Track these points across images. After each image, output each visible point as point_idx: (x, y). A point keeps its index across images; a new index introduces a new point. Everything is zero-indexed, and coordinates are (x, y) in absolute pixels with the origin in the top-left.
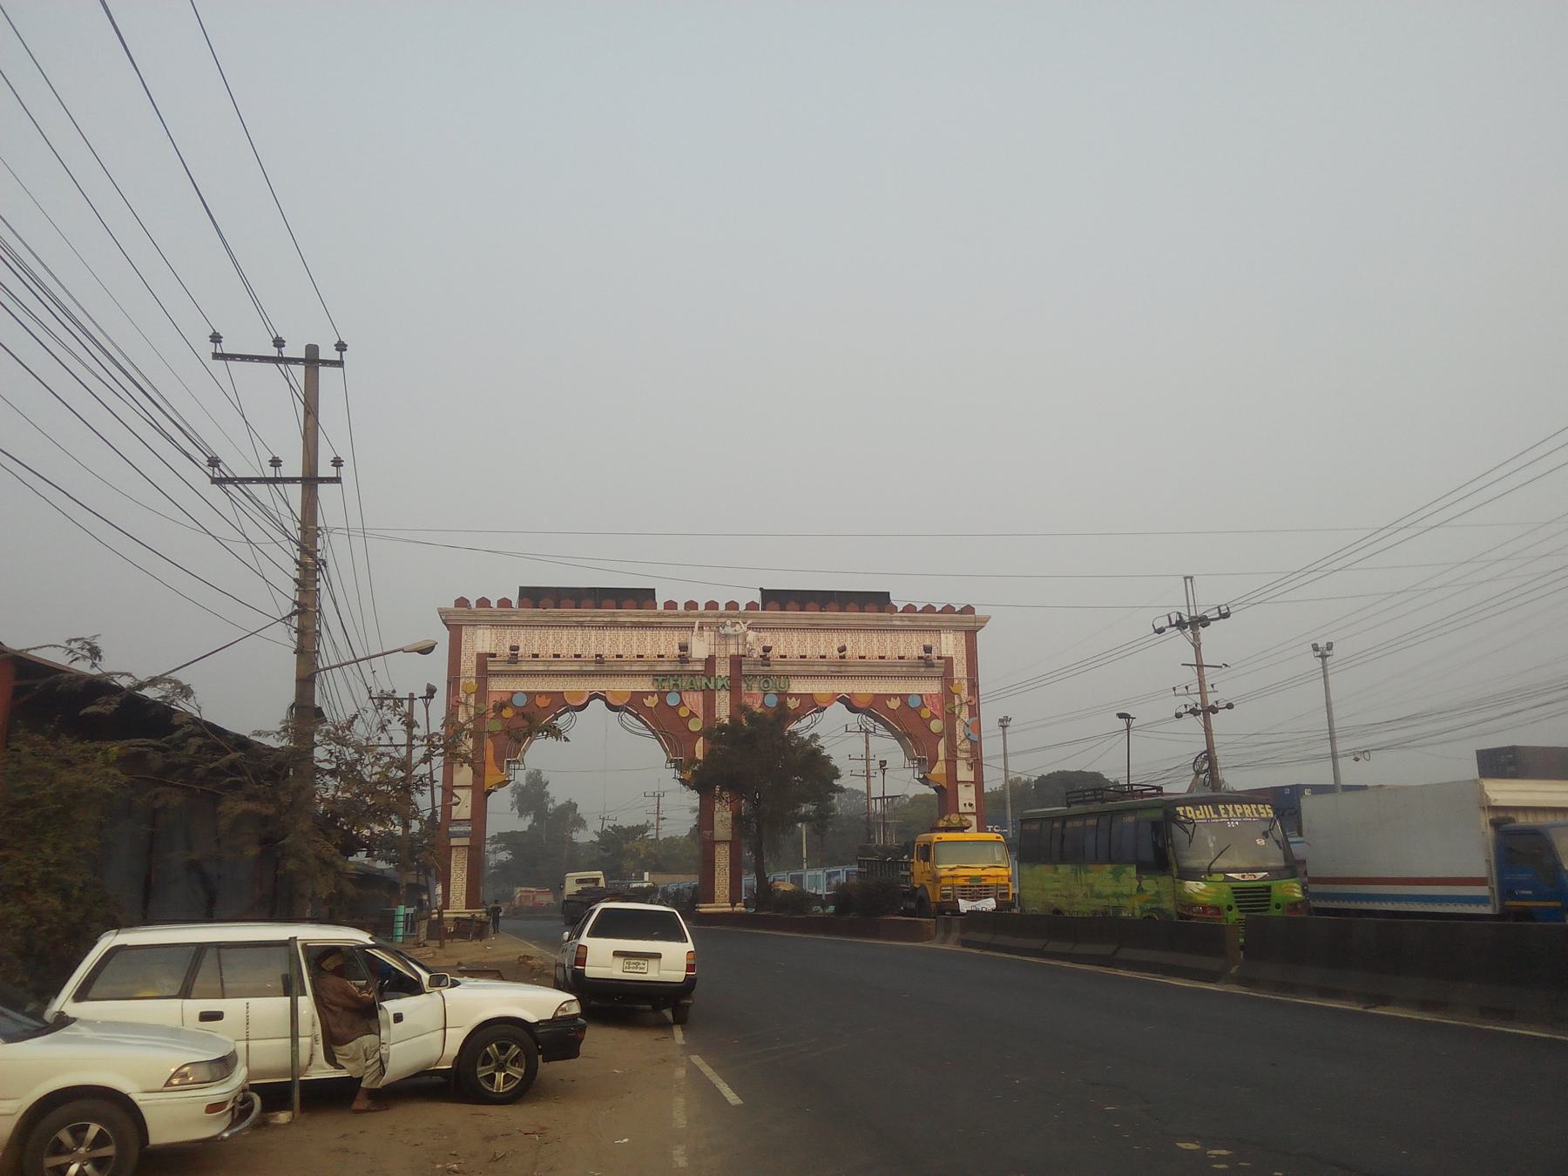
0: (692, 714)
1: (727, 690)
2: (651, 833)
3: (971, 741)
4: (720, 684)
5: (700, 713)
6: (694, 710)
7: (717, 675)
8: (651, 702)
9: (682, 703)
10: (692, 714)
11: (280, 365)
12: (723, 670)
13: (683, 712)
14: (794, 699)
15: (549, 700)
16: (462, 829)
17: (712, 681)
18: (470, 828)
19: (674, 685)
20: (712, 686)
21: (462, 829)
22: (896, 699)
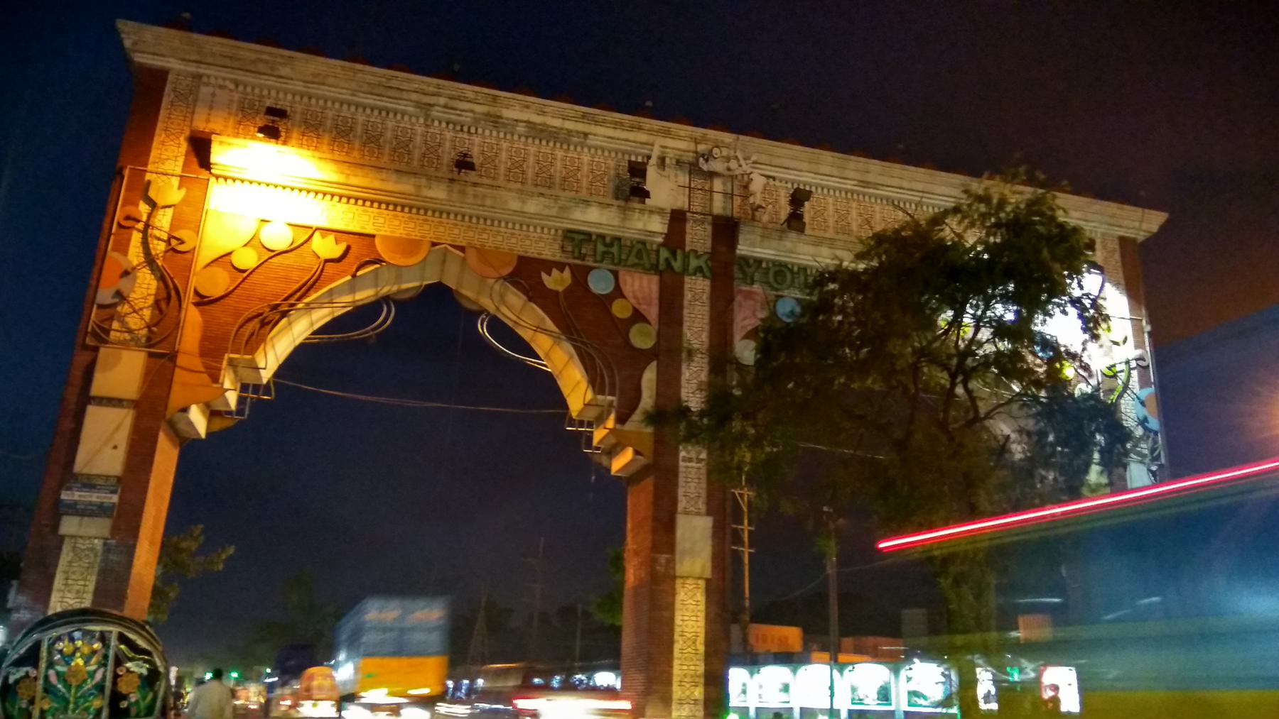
0: (638, 316)
1: (704, 276)
2: (690, 414)
3: (578, 685)
4: (694, 263)
5: (653, 312)
6: (643, 308)
7: (688, 249)
8: (556, 281)
9: (618, 292)
10: (638, 316)
11: (908, 218)
12: (698, 237)
13: (620, 310)
14: (555, 272)
15: (342, 247)
16: (94, 497)
17: (679, 257)
18: (115, 498)
19: (604, 253)
20: (677, 265)
21: (94, 497)
22: (562, 271)
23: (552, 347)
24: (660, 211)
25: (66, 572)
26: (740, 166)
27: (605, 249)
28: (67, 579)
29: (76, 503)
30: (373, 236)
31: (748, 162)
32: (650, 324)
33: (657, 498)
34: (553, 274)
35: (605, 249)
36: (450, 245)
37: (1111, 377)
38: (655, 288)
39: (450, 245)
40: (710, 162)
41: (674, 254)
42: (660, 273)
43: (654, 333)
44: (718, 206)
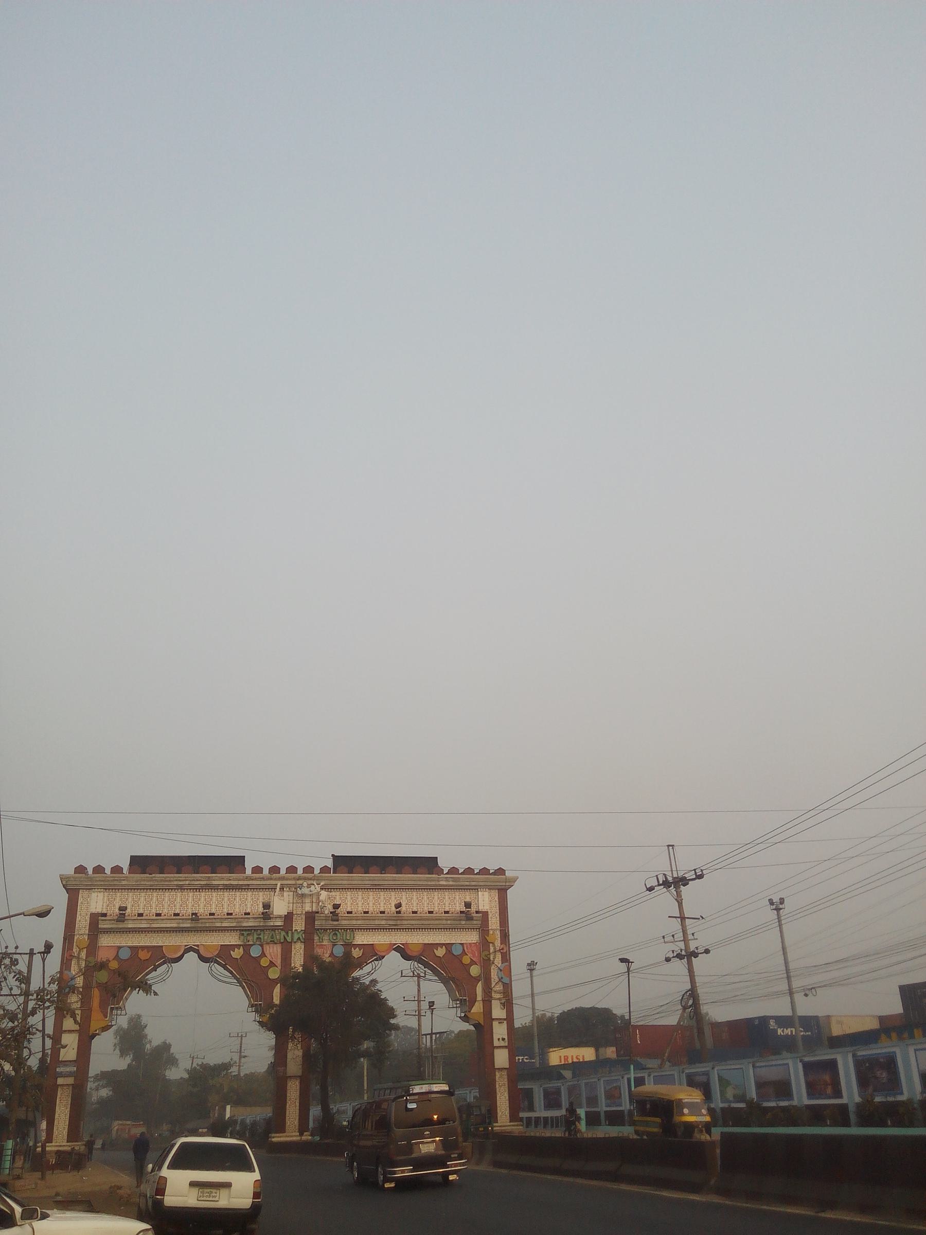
0: (272, 964)
1: (302, 942)
4: (296, 937)
5: (278, 962)
7: (294, 929)
9: (263, 955)
10: (272, 964)
12: (299, 925)
13: (264, 962)
16: (68, 1069)
17: (290, 935)
20: (289, 939)
21: (68, 1069)
23: (419, 985)
24: (280, 917)
25: (60, 1098)
26: (316, 888)
27: (257, 936)
28: (61, 1100)
29: (62, 1072)
30: (162, 947)
31: (319, 886)
32: (277, 967)
33: (43, 1023)
34: (439, 950)
35: (260, 936)
36: (400, 944)
37: (487, 960)
38: (279, 950)
39: (400, 944)
40: (302, 889)
41: (287, 933)
42: (282, 943)
43: (279, 971)
44: (308, 908)
